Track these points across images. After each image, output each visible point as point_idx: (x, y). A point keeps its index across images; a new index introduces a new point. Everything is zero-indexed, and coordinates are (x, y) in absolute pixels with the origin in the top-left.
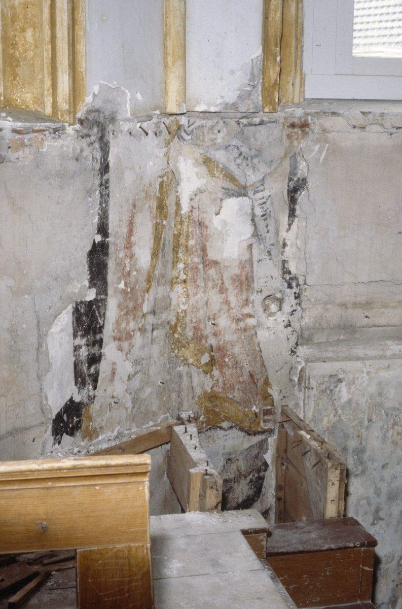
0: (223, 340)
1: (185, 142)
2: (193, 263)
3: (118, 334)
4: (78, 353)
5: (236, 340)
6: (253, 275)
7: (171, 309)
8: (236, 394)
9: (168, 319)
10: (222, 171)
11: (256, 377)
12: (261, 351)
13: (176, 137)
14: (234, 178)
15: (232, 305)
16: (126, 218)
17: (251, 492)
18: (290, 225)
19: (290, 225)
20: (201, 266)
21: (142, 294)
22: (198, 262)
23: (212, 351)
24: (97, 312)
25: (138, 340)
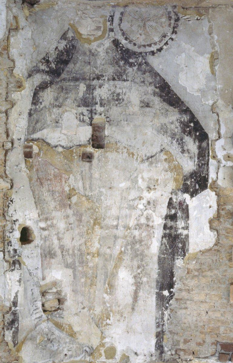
0: (62, 212)
1: (87, 345)
2: (83, 266)
3: (149, 229)
4: (185, 225)
5: (53, 212)
6: (41, 258)
7: (99, 237)
8: (53, 172)
9: (102, 230)
10: (63, 330)
11: (38, 183)
12: (35, 203)
13: (94, 349)
14: (55, 325)
15: (56, 237)
16: (140, 302)
17: (41, 94)
18: (16, 296)
19: (16, 296)
20: (77, 264)
21: (126, 251)
22: (79, 267)
23: (69, 204)
24: (168, 247)
25: (132, 223)
